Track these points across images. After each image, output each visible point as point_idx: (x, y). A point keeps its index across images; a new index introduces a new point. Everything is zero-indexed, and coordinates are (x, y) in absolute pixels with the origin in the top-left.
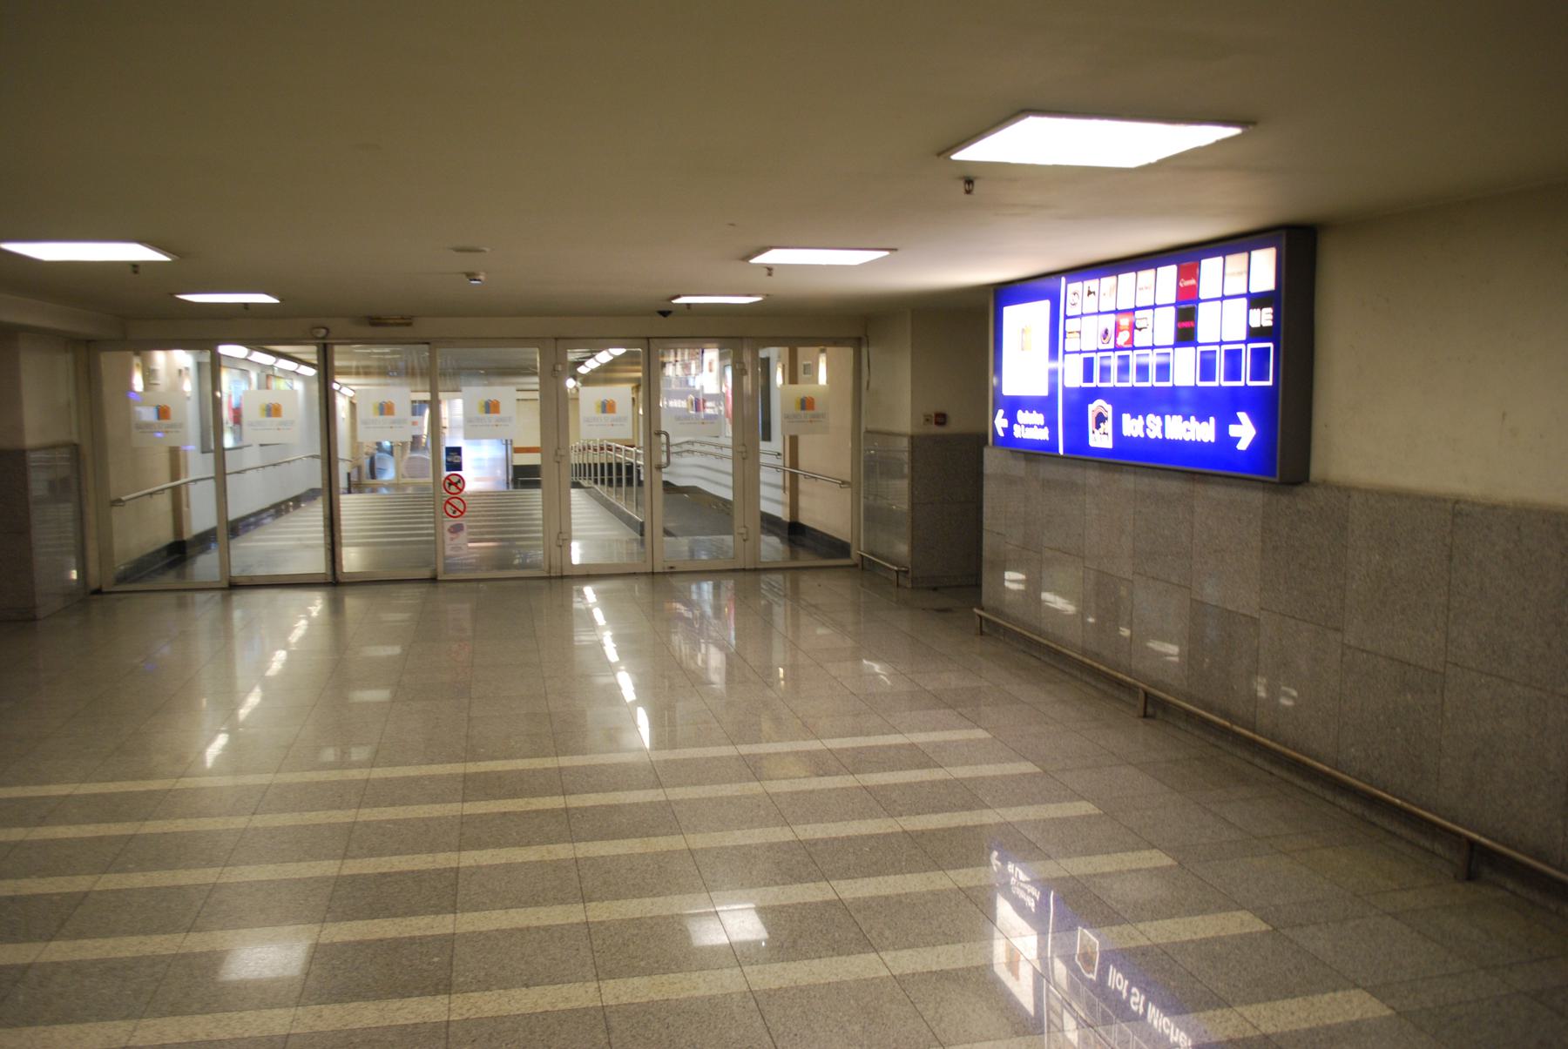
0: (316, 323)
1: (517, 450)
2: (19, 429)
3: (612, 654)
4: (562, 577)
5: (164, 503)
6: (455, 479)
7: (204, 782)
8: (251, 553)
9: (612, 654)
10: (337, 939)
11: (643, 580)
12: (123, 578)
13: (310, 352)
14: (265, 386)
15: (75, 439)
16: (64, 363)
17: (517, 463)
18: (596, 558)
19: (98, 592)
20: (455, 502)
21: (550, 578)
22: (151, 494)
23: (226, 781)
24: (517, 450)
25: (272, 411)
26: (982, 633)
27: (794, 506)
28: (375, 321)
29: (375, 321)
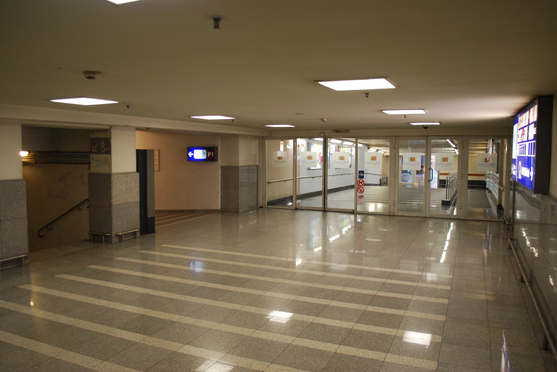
0: (308, 132)
1: (441, 174)
2: (238, 161)
3: (446, 248)
4: (394, 216)
5: (290, 183)
6: (361, 181)
7: (296, 270)
8: (334, 201)
9: (446, 248)
10: (65, 317)
11: (387, 217)
12: (271, 203)
13: (321, 139)
14: (310, 150)
15: (258, 164)
16: (255, 144)
17: (440, 178)
18: (525, 218)
19: (262, 207)
20: (361, 188)
21: (390, 215)
22: (285, 181)
23: (301, 271)
24: (441, 174)
25: (342, 158)
26: (51, 229)
27: (352, 187)
28: (337, 131)
29: (337, 131)
